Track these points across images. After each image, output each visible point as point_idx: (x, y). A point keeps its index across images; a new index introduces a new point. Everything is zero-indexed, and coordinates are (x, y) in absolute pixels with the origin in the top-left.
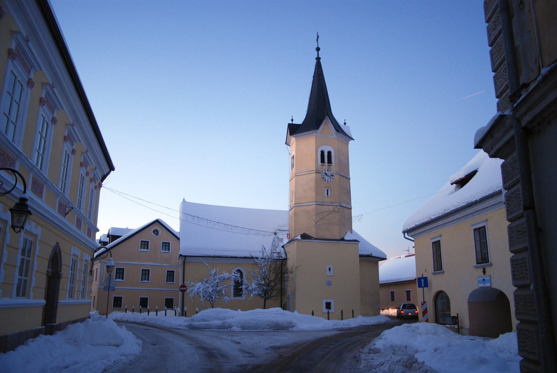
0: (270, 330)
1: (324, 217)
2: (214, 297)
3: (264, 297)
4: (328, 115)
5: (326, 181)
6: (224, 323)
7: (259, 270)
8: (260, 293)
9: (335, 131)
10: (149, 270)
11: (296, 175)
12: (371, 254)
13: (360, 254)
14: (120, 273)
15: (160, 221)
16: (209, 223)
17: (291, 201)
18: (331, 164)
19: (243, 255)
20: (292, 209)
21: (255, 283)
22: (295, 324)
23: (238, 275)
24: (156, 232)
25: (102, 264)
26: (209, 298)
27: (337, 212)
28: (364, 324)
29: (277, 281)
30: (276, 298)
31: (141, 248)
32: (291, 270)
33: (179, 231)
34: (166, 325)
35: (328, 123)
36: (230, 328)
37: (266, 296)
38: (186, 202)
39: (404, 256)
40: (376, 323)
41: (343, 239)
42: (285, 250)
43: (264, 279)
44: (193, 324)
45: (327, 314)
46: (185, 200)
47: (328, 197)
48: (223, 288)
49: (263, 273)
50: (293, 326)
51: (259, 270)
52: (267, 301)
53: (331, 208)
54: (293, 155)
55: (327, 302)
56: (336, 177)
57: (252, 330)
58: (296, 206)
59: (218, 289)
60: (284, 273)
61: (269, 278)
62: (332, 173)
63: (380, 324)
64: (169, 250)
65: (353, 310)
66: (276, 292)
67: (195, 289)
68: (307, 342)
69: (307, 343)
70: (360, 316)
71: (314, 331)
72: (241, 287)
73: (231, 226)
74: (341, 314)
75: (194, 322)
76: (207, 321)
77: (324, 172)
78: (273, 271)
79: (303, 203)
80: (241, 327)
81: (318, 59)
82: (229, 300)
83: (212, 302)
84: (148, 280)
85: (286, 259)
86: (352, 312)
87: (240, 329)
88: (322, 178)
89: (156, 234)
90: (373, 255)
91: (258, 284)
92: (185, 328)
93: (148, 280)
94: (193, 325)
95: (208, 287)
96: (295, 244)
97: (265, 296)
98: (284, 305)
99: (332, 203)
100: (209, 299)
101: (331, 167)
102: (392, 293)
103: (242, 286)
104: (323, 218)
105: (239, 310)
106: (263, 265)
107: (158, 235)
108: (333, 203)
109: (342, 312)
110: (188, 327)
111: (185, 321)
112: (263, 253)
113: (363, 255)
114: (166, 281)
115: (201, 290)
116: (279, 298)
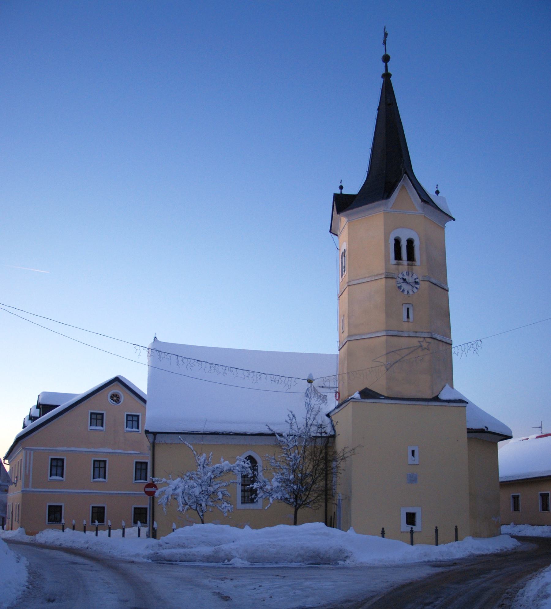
0: (303, 565)
1: (403, 358)
2: (204, 505)
3: (293, 503)
4: (406, 173)
5: (406, 292)
6: (217, 552)
7: (283, 455)
8: (287, 496)
9: (420, 200)
10: (105, 462)
11: (350, 284)
12: (486, 428)
13: (470, 428)
14: (57, 466)
15: (121, 378)
16: (181, 363)
17: (341, 333)
18: (413, 262)
19: (256, 431)
20: (343, 346)
21: (277, 479)
22: (350, 554)
23: (248, 464)
24: (116, 398)
25: (27, 452)
26: (195, 505)
27: (426, 348)
28: (478, 553)
29: (318, 475)
30: (316, 505)
31: (91, 425)
32: (341, 454)
33: (146, 392)
34: (115, 554)
35: (407, 188)
36: (229, 560)
37: (298, 502)
38: (160, 342)
39: (535, 436)
40: (497, 550)
41: (436, 399)
42: (332, 421)
43: (293, 471)
44: (160, 554)
45: (409, 535)
46: (158, 339)
47: (408, 322)
48: (219, 487)
49: (292, 461)
50: (347, 557)
51: (283, 455)
52: (300, 511)
53: (415, 342)
54: (343, 251)
55: (407, 512)
56: (424, 286)
57: (268, 565)
58: (350, 339)
59: (211, 489)
60: (332, 461)
61: (302, 470)
62: (415, 279)
63: (506, 552)
64: (138, 428)
65: (456, 527)
66: (316, 495)
67: (169, 490)
68: (372, 597)
69: (374, 600)
70: (468, 537)
71: (386, 567)
72: (251, 486)
73: (223, 367)
74: (434, 533)
75: (163, 549)
76: (187, 547)
77: (401, 276)
78: (310, 457)
79: (364, 334)
80: (248, 559)
81: (387, 76)
82: (230, 509)
83: (201, 514)
84: (105, 478)
85: (334, 436)
86: (454, 531)
87: (247, 564)
88: (397, 289)
89: (116, 402)
90: (490, 429)
91: (283, 480)
92: (145, 560)
93: (105, 478)
94: (160, 555)
95: (193, 487)
96: (349, 408)
97: (296, 502)
98: (331, 517)
99: (416, 332)
100: (196, 508)
101: (414, 267)
102: (516, 498)
103: (253, 485)
104: (399, 360)
105: (247, 528)
106: (291, 446)
107: (120, 402)
108: (417, 334)
109: (437, 531)
110: (151, 559)
111: (147, 547)
112: (291, 424)
113: (472, 429)
114: (134, 479)
115: (179, 491)
116: (321, 506)
